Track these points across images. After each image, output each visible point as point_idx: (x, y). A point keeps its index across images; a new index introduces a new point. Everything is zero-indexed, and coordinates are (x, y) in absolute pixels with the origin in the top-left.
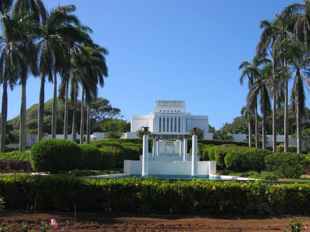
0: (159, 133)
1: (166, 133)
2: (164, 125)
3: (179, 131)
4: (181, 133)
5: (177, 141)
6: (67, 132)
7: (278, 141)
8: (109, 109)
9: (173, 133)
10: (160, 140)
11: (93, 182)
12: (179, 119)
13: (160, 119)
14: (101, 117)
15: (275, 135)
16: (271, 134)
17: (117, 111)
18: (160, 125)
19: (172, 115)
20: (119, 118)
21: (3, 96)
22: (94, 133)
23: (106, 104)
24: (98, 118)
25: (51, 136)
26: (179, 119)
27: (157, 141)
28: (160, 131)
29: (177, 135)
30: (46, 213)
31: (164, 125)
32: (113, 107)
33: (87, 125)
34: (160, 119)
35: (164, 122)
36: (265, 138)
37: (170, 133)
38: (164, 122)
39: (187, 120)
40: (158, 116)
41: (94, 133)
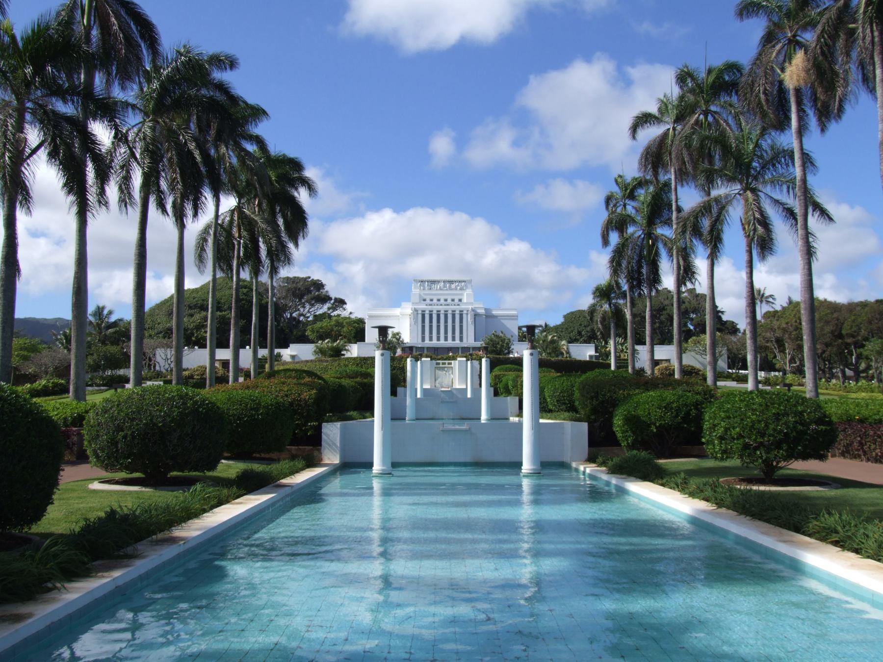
0: (420, 344)
1: (435, 343)
2: (431, 327)
3: (461, 339)
4: (465, 344)
5: (458, 359)
6: (215, 342)
7: (657, 357)
8: (325, 299)
9: (450, 343)
10: (423, 359)
11: (611, 563)
12: (461, 316)
13: (423, 316)
14: (309, 315)
15: (652, 345)
16: (644, 343)
17: (341, 302)
18: (423, 327)
19: (439, 308)
20: (345, 314)
21: (864, 305)
22: (291, 345)
23: (318, 290)
24: (304, 316)
25: (206, 352)
26: (461, 316)
27: (419, 362)
28: (423, 339)
29: (458, 348)
30: (152, 568)
31: (438, 327)
32: (333, 295)
33: (269, 328)
34: (423, 316)
35: (446, 321)
36: (634, 351)
37: (442, 343)
38: (446, 321)
39: (477, 318)
40: (420, 312)
41: (291, 345)
